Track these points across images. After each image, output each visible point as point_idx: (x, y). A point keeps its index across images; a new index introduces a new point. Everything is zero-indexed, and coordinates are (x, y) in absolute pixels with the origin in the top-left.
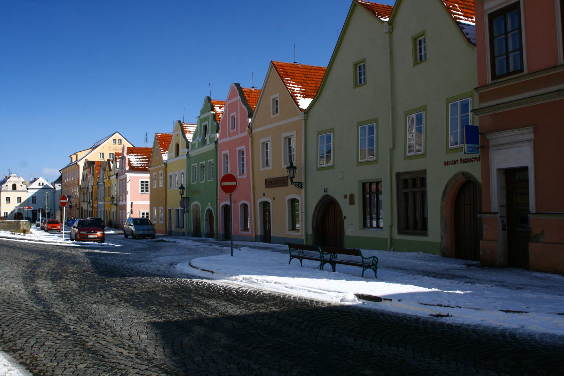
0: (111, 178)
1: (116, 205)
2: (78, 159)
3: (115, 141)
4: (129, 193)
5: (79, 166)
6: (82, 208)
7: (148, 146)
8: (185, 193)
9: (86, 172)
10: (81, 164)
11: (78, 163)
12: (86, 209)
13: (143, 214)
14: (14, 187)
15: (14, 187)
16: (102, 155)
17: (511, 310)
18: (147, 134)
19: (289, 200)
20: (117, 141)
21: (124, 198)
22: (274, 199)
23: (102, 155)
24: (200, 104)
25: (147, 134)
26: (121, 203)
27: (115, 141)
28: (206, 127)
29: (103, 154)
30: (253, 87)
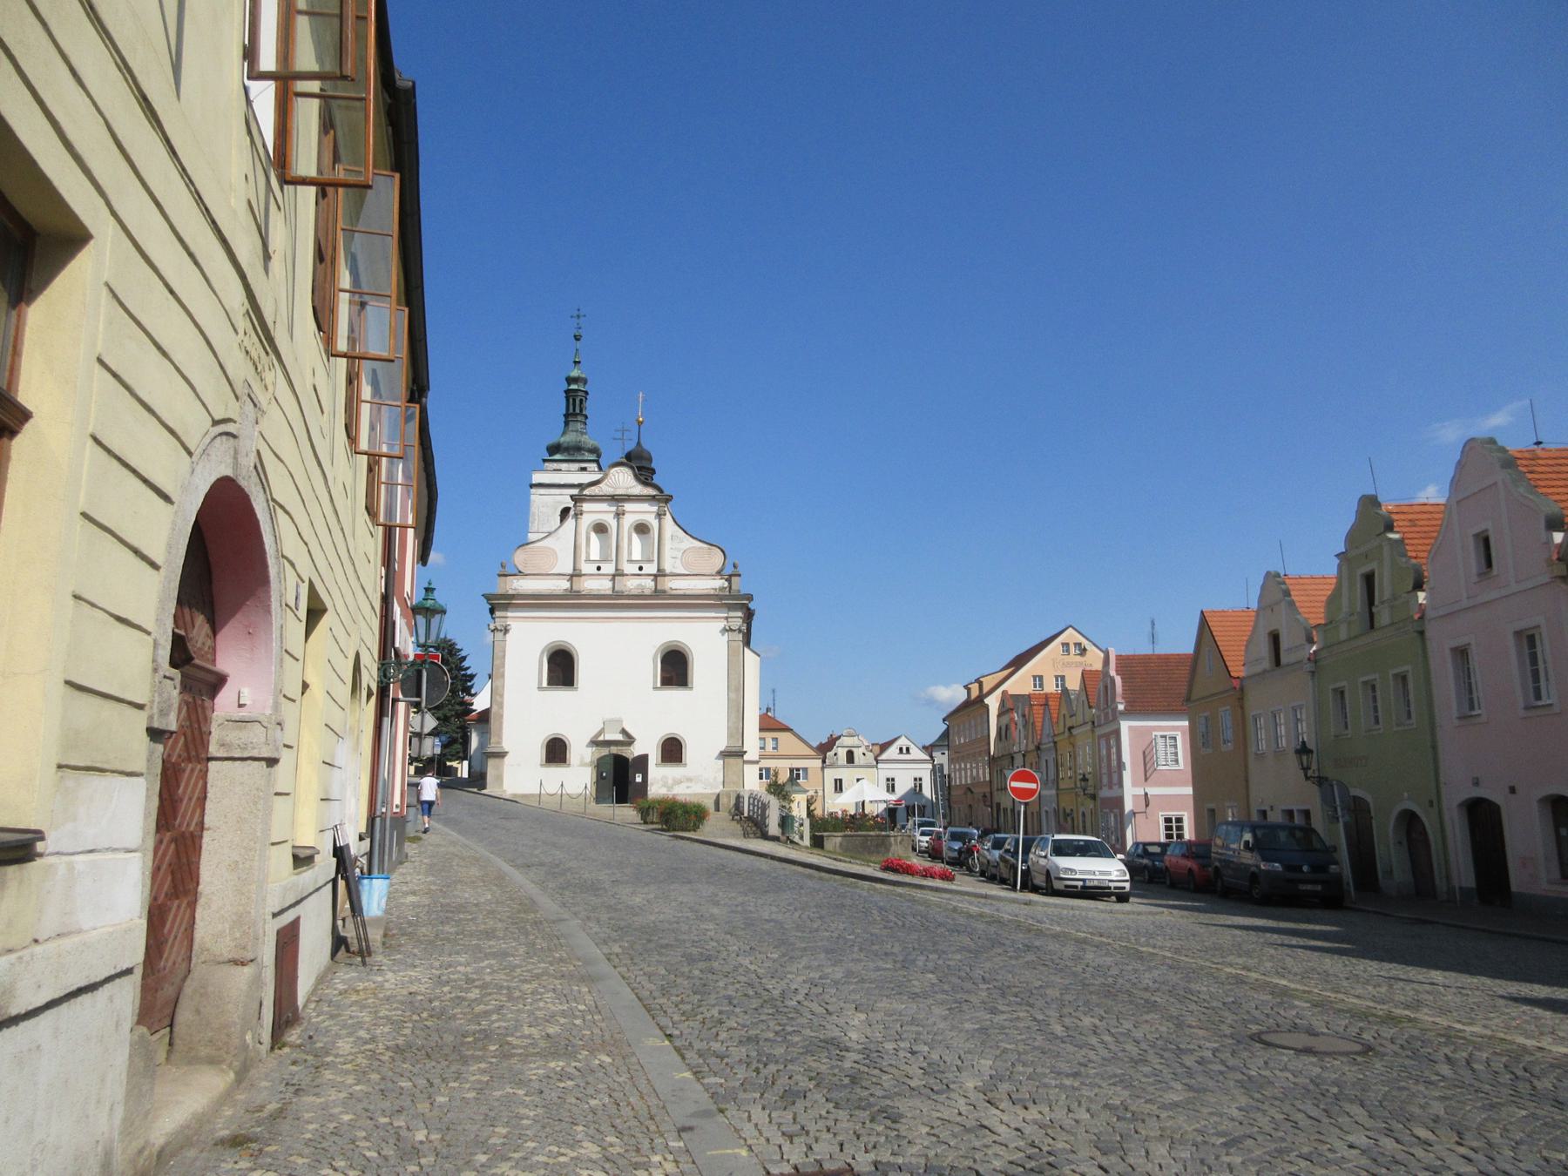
0: (1074, 732)
1: (1093, 797)
2: (985, 690)
3: (1066, 645)
4: (1128, 766)
5: (987, 707)
6: (998, 805)
7: (1164, 648)
8: (1314, 766)
9: (1005, 719)
10: (993, 702)
11: (986, 701)
12: (1009, 806)
13: (1290, 813)
14: (850, 757)
15: (850, 757)
16: (1038, 679)
17: (73, 763)
18: (1153, 624)
19: (1461, 805)
20: (1072, 648)
21: (1115, 777)
22: (1513, 790)
23: (1038, 679)
24: (1345, 519)
25: (1153, 624)
26: (1105, 793)
27: (1066, 645)
28: (1369, 579)
29: (1041, 678)
30: (1538, 443)
